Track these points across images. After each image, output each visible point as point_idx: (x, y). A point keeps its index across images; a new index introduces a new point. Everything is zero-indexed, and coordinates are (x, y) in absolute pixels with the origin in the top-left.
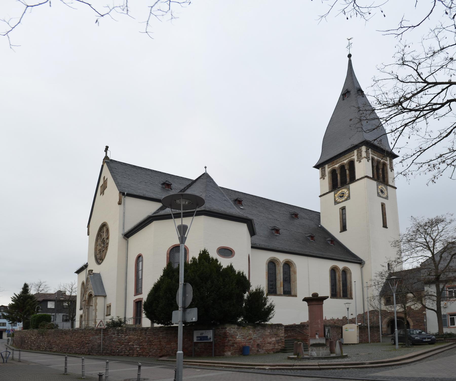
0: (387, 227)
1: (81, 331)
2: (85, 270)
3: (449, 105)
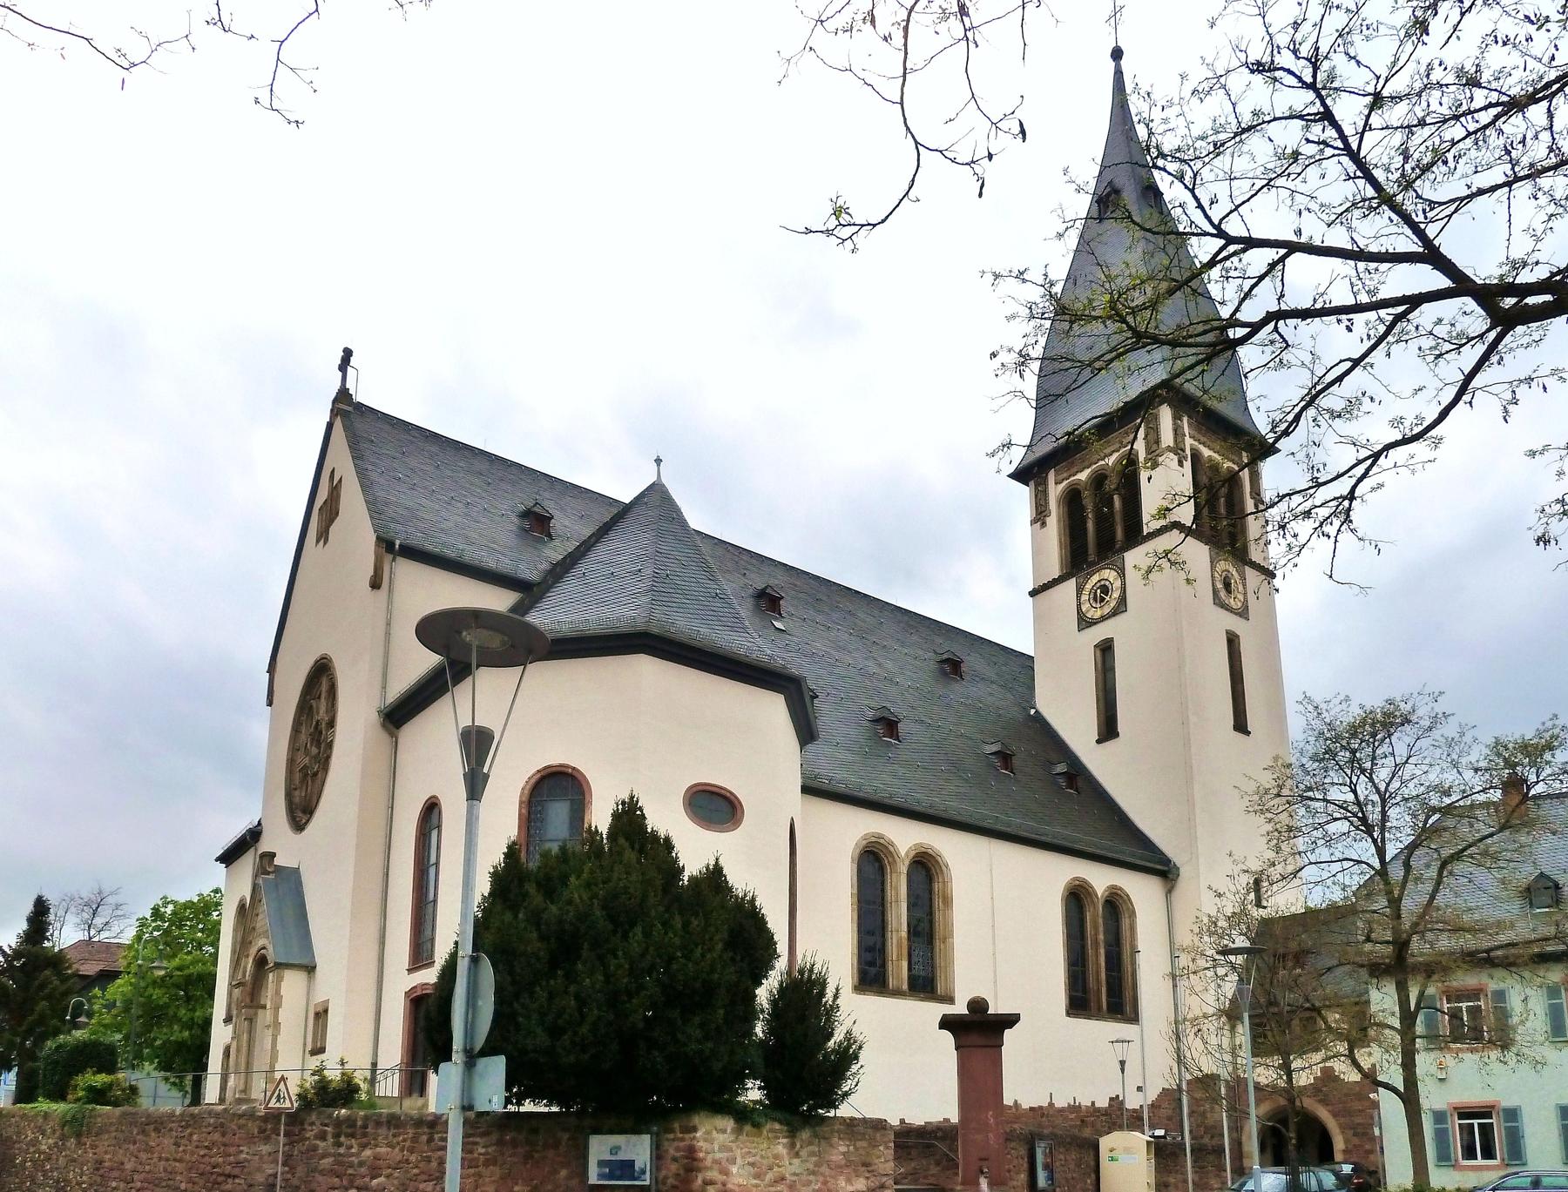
1: (212, 1121)
2: (252, 849)
3: (1276, 329)
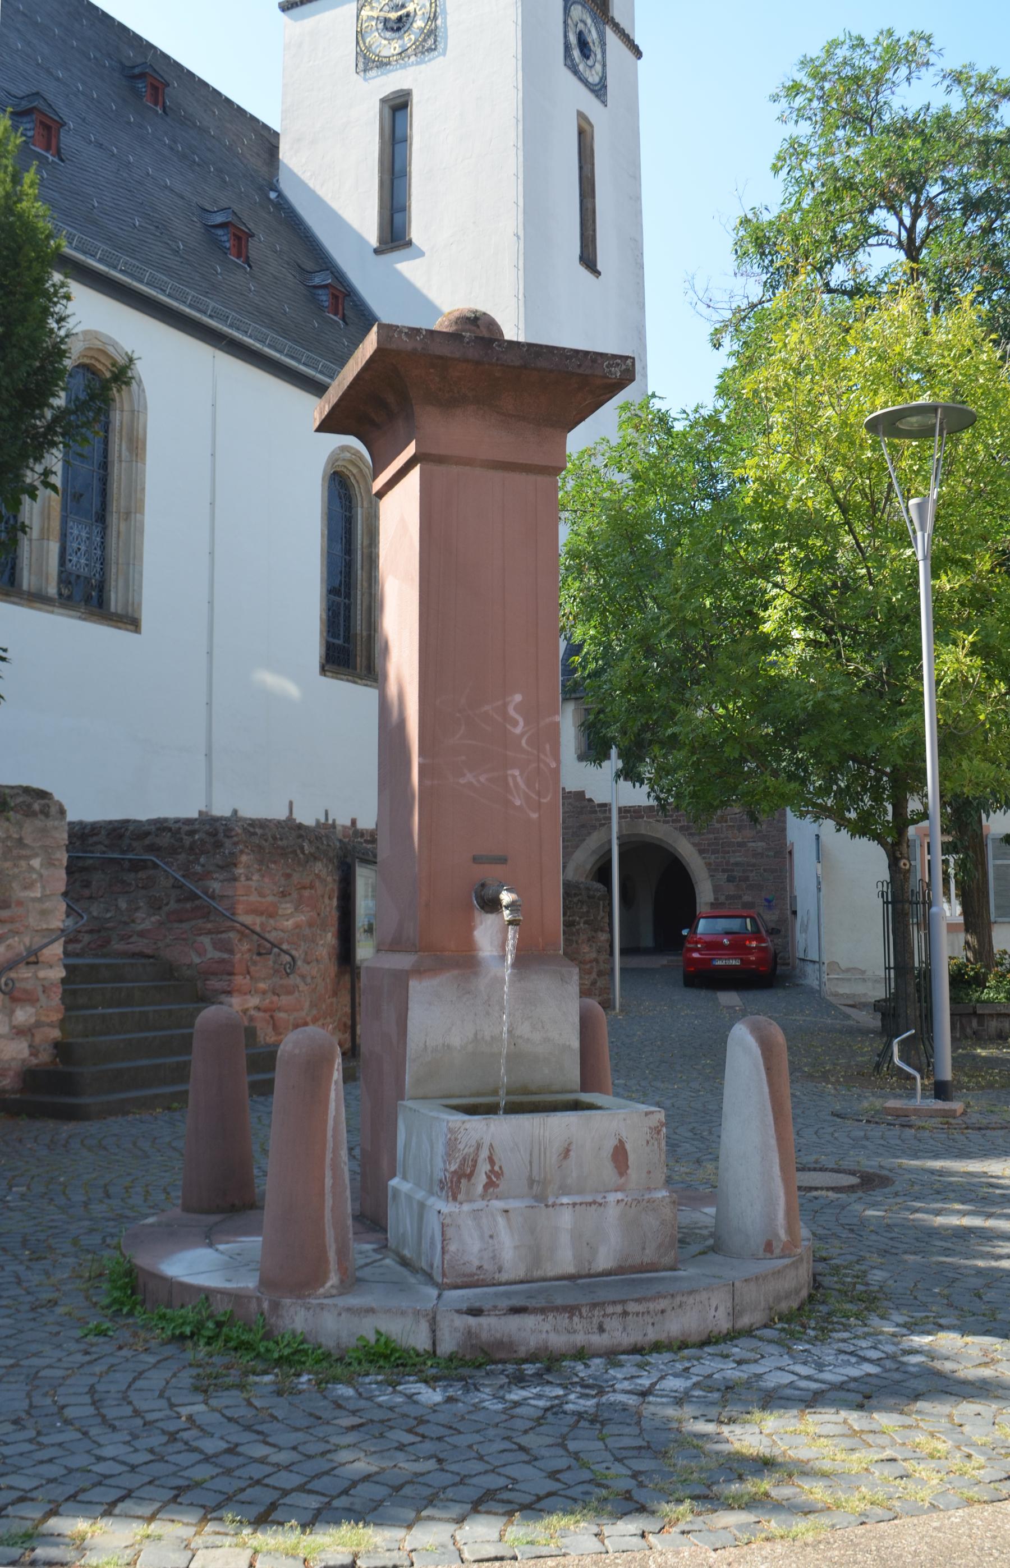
0: (599, 267)
